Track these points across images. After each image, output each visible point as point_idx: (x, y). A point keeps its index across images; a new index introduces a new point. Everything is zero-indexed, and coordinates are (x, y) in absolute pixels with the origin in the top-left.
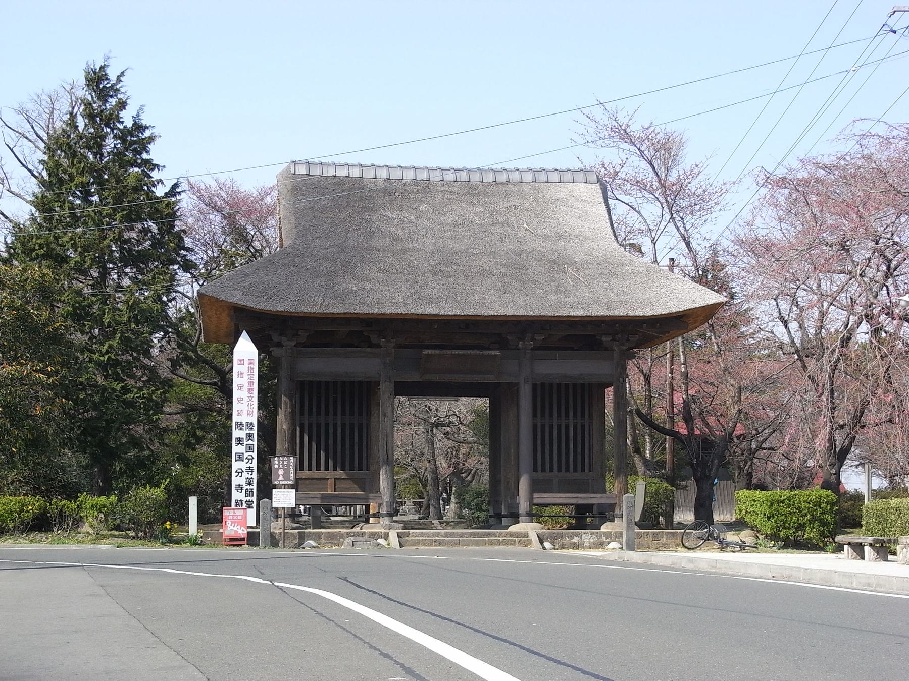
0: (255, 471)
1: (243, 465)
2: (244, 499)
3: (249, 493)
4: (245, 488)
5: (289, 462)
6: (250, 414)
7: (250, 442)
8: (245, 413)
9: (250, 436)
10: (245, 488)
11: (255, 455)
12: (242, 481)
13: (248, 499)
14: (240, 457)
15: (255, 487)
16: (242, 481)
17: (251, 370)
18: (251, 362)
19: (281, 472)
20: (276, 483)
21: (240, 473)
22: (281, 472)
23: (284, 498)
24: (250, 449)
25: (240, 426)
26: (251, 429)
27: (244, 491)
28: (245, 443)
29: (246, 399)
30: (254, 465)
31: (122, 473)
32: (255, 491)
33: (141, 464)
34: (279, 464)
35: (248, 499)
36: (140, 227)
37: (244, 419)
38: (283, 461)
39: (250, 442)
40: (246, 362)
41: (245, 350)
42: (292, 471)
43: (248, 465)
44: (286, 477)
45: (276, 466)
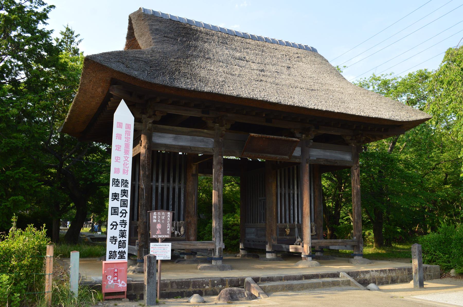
0: (128, 224)
1: (117, 219)
2: (118, 250)
3: (122, 244)
4: (119, 240)
5: (166, 218)
6: (125, 172)
7: (124, 198)
8: (121, 171)
9: (124, 192)
10: (119, 240)
11: (128, 209)
12: (116, 233)
13: (121, 249)
14: (115, 211)
15: (127, 239)
16: (116, 233)
17: (127, 133)
18: (128, 126)
19: (159, 226)
20: (154, 236)
21: (115, 225)
22: (159, 226)
23: (161, 251)
24: (124, 204)
25: (116, 182)
26: (126, 186)
27: (117, 243)
28: (120, 198)
29: (122, 159)
30: (127, 219)
31: (343, 206)
32: (127, 242)
33: (376, 80)
34: (157, 219)
35: (121, 249)
36: (16, 158)
37: (120, 177)
38: (161, 216)
39: (124, 198)
40: (124, 126)
41: (123, 117)
42: (169, 225)
43: (122, 218)
44: (164, 231)
45: (155, 221)
